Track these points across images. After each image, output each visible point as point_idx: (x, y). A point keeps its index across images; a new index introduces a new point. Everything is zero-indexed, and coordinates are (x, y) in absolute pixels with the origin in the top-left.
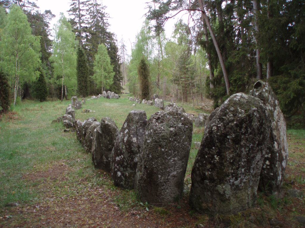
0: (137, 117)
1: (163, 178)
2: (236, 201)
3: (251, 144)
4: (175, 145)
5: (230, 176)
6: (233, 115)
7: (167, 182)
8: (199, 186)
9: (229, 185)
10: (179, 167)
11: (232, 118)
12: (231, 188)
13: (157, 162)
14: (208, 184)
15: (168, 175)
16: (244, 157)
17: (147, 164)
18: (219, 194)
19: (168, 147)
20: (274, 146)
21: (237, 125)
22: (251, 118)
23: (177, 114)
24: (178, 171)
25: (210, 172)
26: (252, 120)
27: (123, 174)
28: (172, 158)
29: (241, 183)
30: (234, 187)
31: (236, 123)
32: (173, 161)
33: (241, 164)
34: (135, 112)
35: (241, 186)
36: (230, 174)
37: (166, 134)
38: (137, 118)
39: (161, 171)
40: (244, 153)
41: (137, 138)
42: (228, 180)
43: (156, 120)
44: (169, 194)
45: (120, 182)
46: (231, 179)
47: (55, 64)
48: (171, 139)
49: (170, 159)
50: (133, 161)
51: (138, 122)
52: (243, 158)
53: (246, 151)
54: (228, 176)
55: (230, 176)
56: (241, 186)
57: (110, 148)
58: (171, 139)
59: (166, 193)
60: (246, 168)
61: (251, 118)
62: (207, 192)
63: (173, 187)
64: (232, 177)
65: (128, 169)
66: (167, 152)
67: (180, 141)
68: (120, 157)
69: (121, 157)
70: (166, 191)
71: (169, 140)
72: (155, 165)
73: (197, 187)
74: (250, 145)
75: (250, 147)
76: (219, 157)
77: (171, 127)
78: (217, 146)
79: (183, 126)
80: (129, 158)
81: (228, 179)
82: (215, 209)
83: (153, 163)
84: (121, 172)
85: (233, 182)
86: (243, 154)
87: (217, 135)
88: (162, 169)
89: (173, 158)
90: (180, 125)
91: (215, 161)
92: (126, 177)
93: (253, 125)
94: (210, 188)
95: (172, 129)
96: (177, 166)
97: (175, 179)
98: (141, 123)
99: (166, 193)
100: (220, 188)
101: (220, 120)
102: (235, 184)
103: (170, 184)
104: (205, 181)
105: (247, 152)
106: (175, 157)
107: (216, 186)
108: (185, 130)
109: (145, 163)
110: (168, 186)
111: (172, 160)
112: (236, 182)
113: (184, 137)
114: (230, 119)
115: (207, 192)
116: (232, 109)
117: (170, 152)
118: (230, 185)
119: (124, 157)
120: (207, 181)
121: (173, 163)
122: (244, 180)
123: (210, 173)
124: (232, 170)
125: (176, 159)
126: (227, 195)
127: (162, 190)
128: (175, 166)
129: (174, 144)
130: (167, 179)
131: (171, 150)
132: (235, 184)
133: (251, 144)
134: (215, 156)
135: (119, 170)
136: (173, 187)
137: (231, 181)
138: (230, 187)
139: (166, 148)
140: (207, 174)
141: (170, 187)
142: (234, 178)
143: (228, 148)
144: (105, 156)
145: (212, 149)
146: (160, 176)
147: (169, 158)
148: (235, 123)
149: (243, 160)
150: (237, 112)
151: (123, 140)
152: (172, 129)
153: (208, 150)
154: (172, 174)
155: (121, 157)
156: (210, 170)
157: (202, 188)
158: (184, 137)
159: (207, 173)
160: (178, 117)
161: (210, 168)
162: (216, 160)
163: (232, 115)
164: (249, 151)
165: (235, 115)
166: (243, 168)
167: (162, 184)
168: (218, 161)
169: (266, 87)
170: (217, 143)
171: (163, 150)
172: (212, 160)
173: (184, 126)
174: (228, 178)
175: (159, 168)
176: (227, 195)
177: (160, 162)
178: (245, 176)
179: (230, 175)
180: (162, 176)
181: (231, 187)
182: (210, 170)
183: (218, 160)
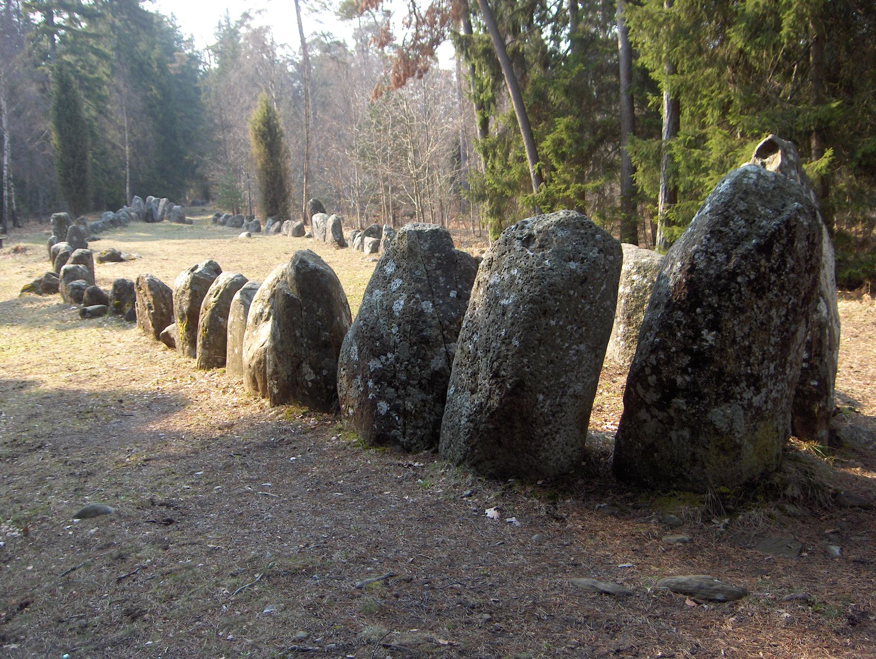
0: (426, 241)
1: (548, 402)
2: (755, 450)
3: (793, 298)
4: (583, 307)
5: (743, 384)
6: (746, 221)
7: (558, 412)
8: (653, 417)
9: (741, 407)
10: (589, 371)
11: (744, 230)
12: (745, 414)
13: (535, 357)
14: (685, 408)
15: (563, 392)
16: (774, 333)
17: (501, 364)
18: (717, 432)
19: (564, 316)
20: (818, 309)
21: (760, 249)
22: (791, 228)
23: (582, 224)
24: (585, 380)
25: (689, 375)
26: (794, 236)
27: (395, 408)
28: (573, 344)
29: (766, 402)
30: (752, 412)
31: (757, 244)
32: (575, 355)
33: (768, 349)
34: (417, 229)
35: (767, 409)
36: (743, 378)
37: (558, 279)
38: (427, 246)
39: (545, 383)
40: (777, 321)
41: (433, 302)
42: (739, 393)
43: (523, 242)
44: (560, 446)
45: (390, 431)
46: (745, 391)
47: (106, 91)
48: (572, 292)
49: (569, 348)
50: (428, 366)
51: (429, 259)
52: (773, 336)
53: (780, 317)
54: (737, 383)
55: (743, 384)
56: (767, 409)
57: (325, 341)
58: (572, 292)
59: (554, 443)
60: (778, 361)
61: (791, 228)
62: (677, 430)
63: (571, 427)
64: (748, 386)
65: (413, 391)
66: (562, 327)
67: (594, 297)
68: (383, 358)
69: (387, 359)
70: (554, 439)
71: (569, 296)
72: (529, 367)
73: (645, 421)
74: (790, 299)
75: (790, 307)
76: (714, 333)
77: (570, 261)
78: (710, 306)
79: (602, 255)
80: (412, 360)
81: (739, 391)
82: (704, 473)
83: (525, 360)
84: (389, 401)
85: (750, 400)
86: (773, 324)
87: (707, 275)
88: (547, 378)
89: (575, 346)
90: (594, 254)
91: (700, 346)
92: (405, 414)
93: (796, 247)
94: (689, 420)
95: (573, 265)
96: (584, 369)
97: (577, 404)
98: (439, 258)
99: (554, 443)
100: (719, 415)
101: (712, 237)
102: (755, 405)
103: (565, 418)
104: (674, 400)
105: (783, 319)
106: (581, 343)
107: (706, 411)
108: (607, 268)
109: (496, 364)
110: (561, 424)
111: (572, 350)
112: (757, 400)
113: (604, 286)
114: (740, 231)
115: (677, 430)
116: (742, 206)
117: (569, 327)
118: (742, 405)
119: (397, 359)
120: (682, 401)
121: (575, 358)
122: (774, 394)
123: (687, 378)
124: (749, 368)
125: (582, 347)
126: (738, 432)
127: (546, 434)
128: (579, 368)
129: (580, 306)
130: (560, 405)
131: (572, 324)
132: (755, 405)
133: (793, 298)
134: (704, 332)
135: (380, 397)
136: (571, 427)
137: (745, 395)
138: (742, 411)
139: (560, 318)
140: (682, 383)
141: (565, 426)
142: (752, 388)
143: (739, 308)
144: (310, 364)
145: (695, 312)
146: (541, 397)
147: (567, 345)
148: (754, 241)
149: (773, 340)
150: (753, 215)
151: (389, 309)
152: (573, 265)
153: (683, 316)
154: (572, 390)
155: (387, 359)
156: (690, 370)
157: (661, 421)
158: (604, 286)
159: (679, 380)
160: (586, 234)
161: (688, 365)
162: (707, 341)
163: (743, 222)
164: (786, 316)
165: (750, 223)
166: (772, 362)
167: (547, 419)
168: (711, 345)
169: (790, 153)
170: (710, 295)
171: (553, 323)
172: (694, 342)
173: (605, 256)
174: (737, 388)
175: (541, 373)
176: (738, 432)
177: (543, 356)
178: (775, 384)
179: (742, 381)
180: (547, 396)
181: (744, 413)
182: (690, 370)
183: (713, 343)
